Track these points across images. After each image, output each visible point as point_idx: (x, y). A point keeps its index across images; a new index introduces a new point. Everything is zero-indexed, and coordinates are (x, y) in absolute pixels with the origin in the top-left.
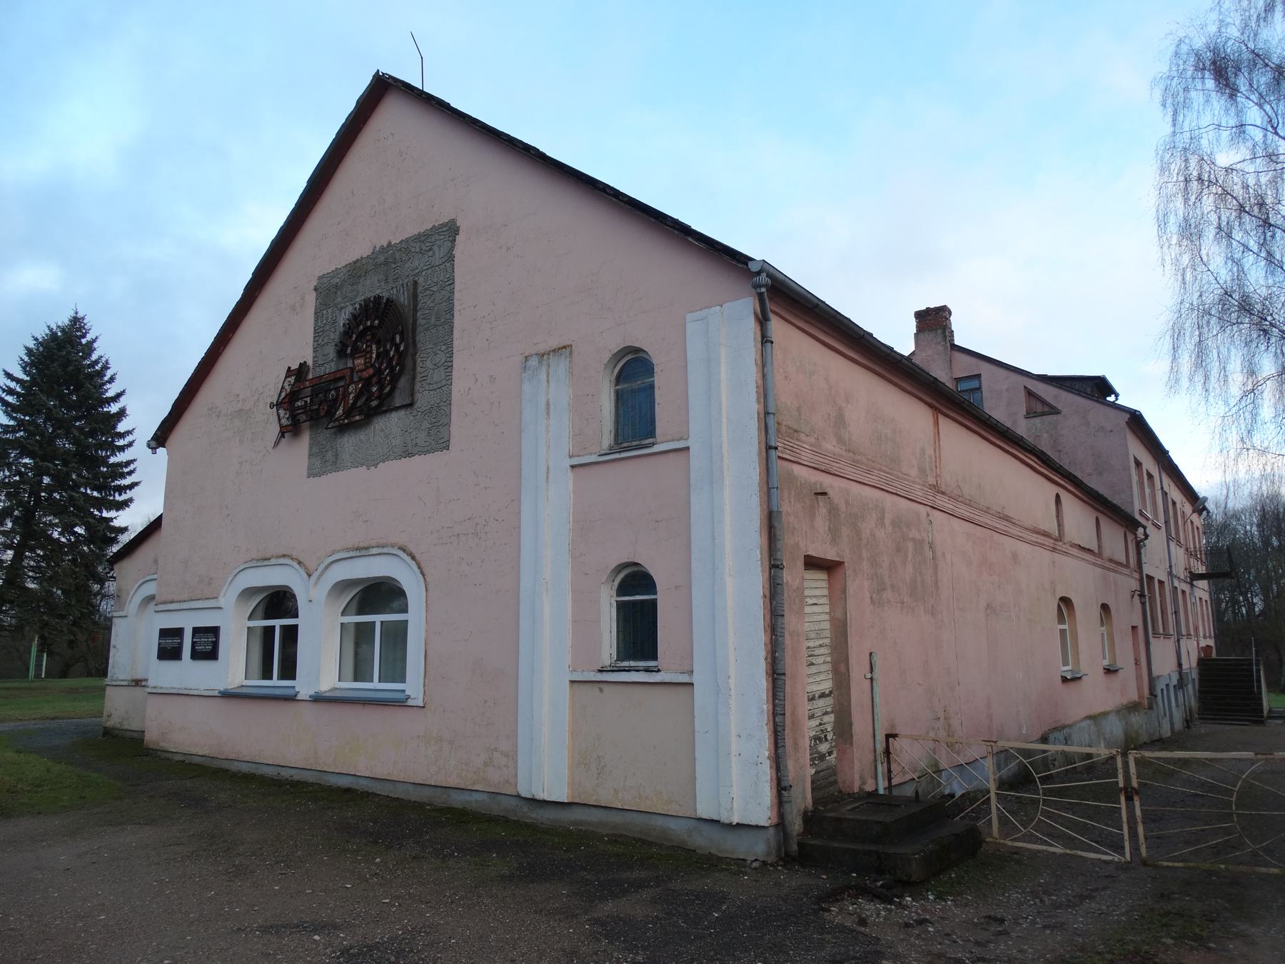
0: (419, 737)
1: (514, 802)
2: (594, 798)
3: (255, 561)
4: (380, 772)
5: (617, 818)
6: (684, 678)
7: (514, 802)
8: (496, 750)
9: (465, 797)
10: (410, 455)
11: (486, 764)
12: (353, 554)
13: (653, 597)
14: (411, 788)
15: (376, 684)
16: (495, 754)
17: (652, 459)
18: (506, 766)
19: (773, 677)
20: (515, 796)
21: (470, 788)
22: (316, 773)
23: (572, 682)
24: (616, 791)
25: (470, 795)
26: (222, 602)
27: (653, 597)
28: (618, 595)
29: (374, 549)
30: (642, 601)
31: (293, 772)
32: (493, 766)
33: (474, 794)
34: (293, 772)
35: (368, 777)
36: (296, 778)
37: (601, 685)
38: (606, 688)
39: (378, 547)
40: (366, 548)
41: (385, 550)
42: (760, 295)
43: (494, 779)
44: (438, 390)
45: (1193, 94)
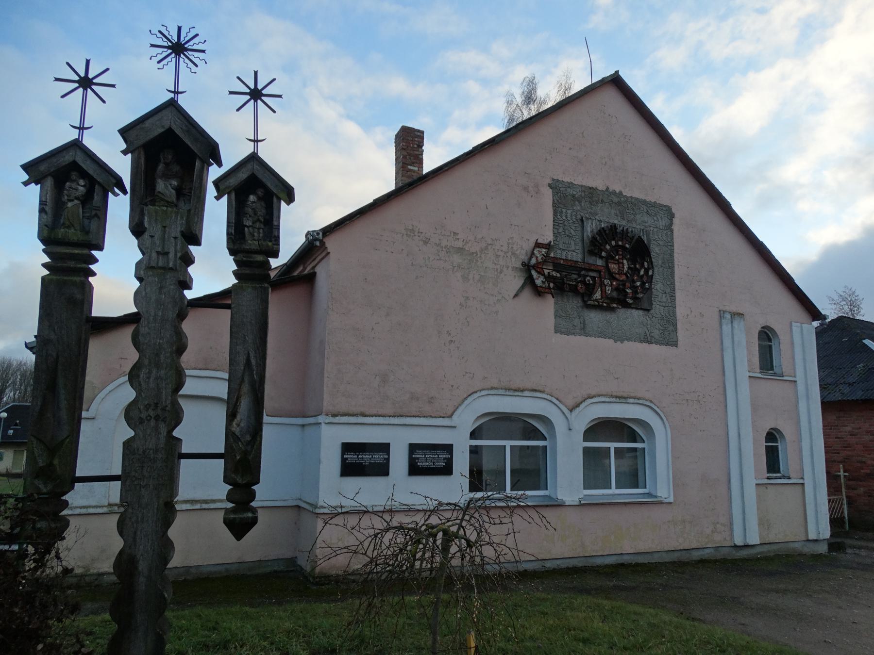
0: (669, 521)
1: (727, 550)
2: (767, 540)
3: (512, 391)
4: (642, 547)
5: (775, 547)
6: (801, 481)
7: (727, 550)
8: (718, 523)
9: (700, 553)
10: (649, 343)
11: (713, 532)
12: (608, 400)
13: (767, 444)
14: (664, 554)
15: (614, 490)
16: (718, 526)
17: (781, 382)
18: (724, 531)
19: (10, 496)
20: (733, 546)
21: (704, 547)
22: (582, 559)
23: (756, 484)
24: (776, 535)
25: (703, 551)
26: (456, 420)
27: (767, 444)
28: (766, 442)
29: (631, 399)
30: (772, 446)
31: (558, 562)
32: (717, 532)
33: (705, 550)
34: (558, 562)
35: (634, 553)
36: (563, 566)
37: (766, 486)
38: (769, 487)
39: (634, 398)
40: (625, 398)
41: (641, 401)
42: (731, 314)
43: (719, 539)
44: (666, 308)
45: (842, 304)
